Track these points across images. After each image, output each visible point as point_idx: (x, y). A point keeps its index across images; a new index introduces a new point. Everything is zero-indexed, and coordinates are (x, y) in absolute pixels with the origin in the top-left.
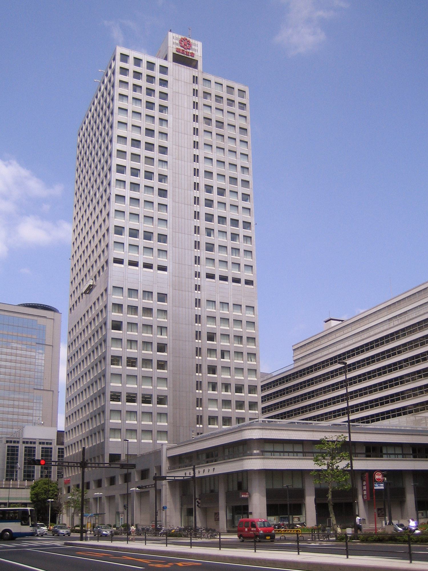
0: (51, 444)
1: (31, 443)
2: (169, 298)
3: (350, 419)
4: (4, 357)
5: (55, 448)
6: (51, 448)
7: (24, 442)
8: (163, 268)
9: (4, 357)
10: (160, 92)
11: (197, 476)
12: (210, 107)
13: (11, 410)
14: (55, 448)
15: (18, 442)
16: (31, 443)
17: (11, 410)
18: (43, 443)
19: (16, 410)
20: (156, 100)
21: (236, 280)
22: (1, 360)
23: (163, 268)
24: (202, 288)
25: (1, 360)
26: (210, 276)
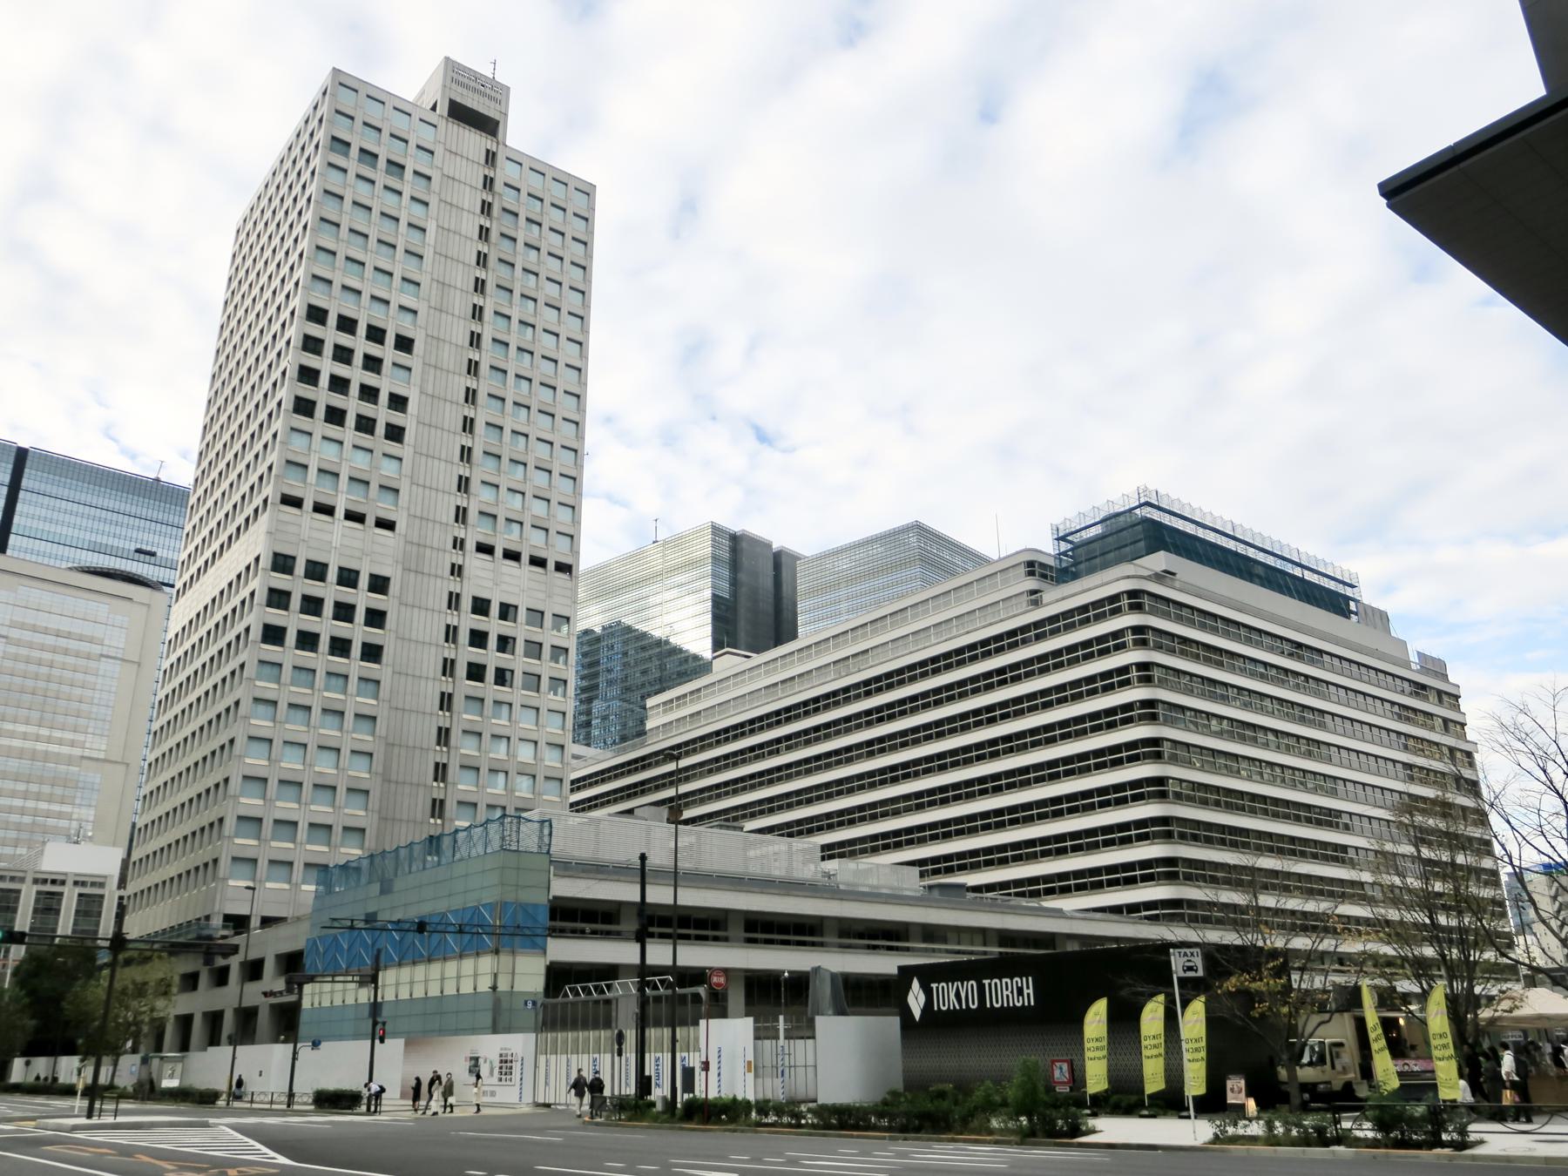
0: (102, 885)
1: (54, 882)
2: (394, 587)
3: (649, 961)
4: (13, 764)
5: (111, 895)
6: (102, 896)
7: (36, 881)
8: (386, 524)
9: (13, 764)
10: (337, 347)
11: (667, 1032)
12: (516, 215)
13: (18, 803)
14: (111, 895)
15: (22, 880)
16: (54, 882)
17: (18, 803)
18: (83, 884)
19: (30, 804)
20: (327, 366)
21: (539, 562)
22: (4, 776)
23: (386, 524)
24: (466, 572)
25: (4, 776)
26: (485, 549)
